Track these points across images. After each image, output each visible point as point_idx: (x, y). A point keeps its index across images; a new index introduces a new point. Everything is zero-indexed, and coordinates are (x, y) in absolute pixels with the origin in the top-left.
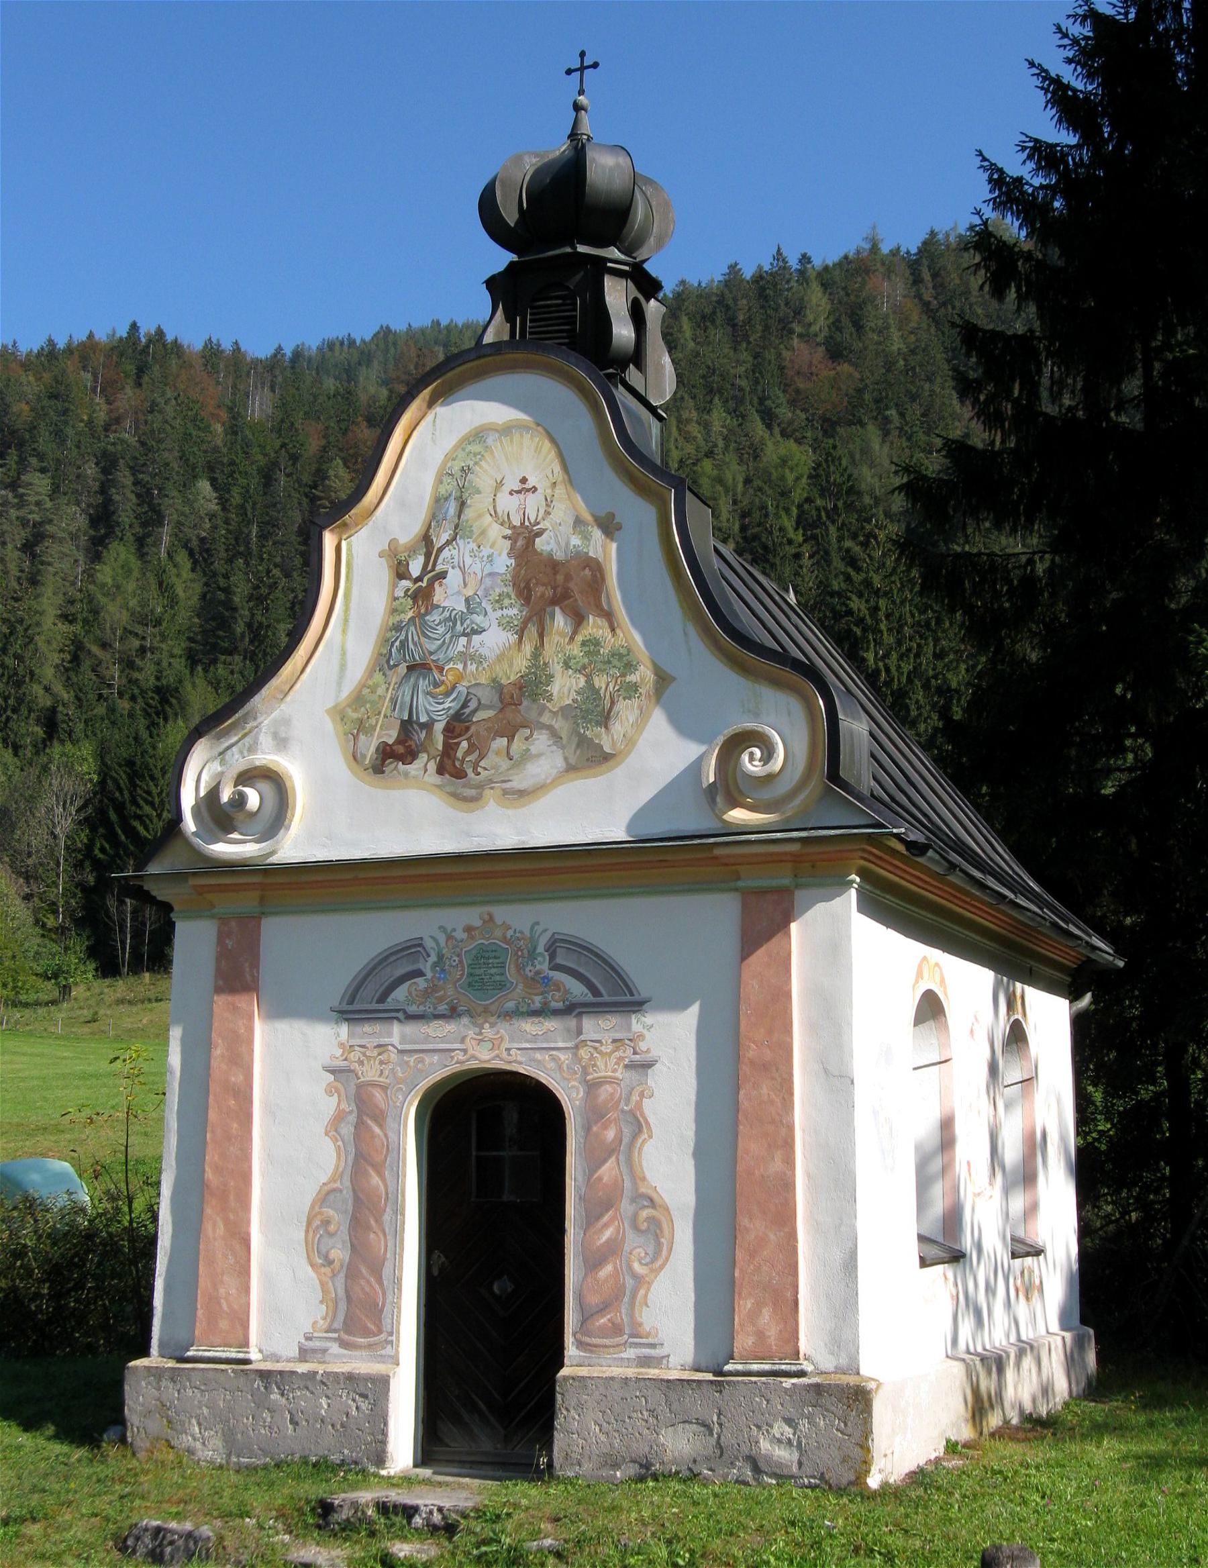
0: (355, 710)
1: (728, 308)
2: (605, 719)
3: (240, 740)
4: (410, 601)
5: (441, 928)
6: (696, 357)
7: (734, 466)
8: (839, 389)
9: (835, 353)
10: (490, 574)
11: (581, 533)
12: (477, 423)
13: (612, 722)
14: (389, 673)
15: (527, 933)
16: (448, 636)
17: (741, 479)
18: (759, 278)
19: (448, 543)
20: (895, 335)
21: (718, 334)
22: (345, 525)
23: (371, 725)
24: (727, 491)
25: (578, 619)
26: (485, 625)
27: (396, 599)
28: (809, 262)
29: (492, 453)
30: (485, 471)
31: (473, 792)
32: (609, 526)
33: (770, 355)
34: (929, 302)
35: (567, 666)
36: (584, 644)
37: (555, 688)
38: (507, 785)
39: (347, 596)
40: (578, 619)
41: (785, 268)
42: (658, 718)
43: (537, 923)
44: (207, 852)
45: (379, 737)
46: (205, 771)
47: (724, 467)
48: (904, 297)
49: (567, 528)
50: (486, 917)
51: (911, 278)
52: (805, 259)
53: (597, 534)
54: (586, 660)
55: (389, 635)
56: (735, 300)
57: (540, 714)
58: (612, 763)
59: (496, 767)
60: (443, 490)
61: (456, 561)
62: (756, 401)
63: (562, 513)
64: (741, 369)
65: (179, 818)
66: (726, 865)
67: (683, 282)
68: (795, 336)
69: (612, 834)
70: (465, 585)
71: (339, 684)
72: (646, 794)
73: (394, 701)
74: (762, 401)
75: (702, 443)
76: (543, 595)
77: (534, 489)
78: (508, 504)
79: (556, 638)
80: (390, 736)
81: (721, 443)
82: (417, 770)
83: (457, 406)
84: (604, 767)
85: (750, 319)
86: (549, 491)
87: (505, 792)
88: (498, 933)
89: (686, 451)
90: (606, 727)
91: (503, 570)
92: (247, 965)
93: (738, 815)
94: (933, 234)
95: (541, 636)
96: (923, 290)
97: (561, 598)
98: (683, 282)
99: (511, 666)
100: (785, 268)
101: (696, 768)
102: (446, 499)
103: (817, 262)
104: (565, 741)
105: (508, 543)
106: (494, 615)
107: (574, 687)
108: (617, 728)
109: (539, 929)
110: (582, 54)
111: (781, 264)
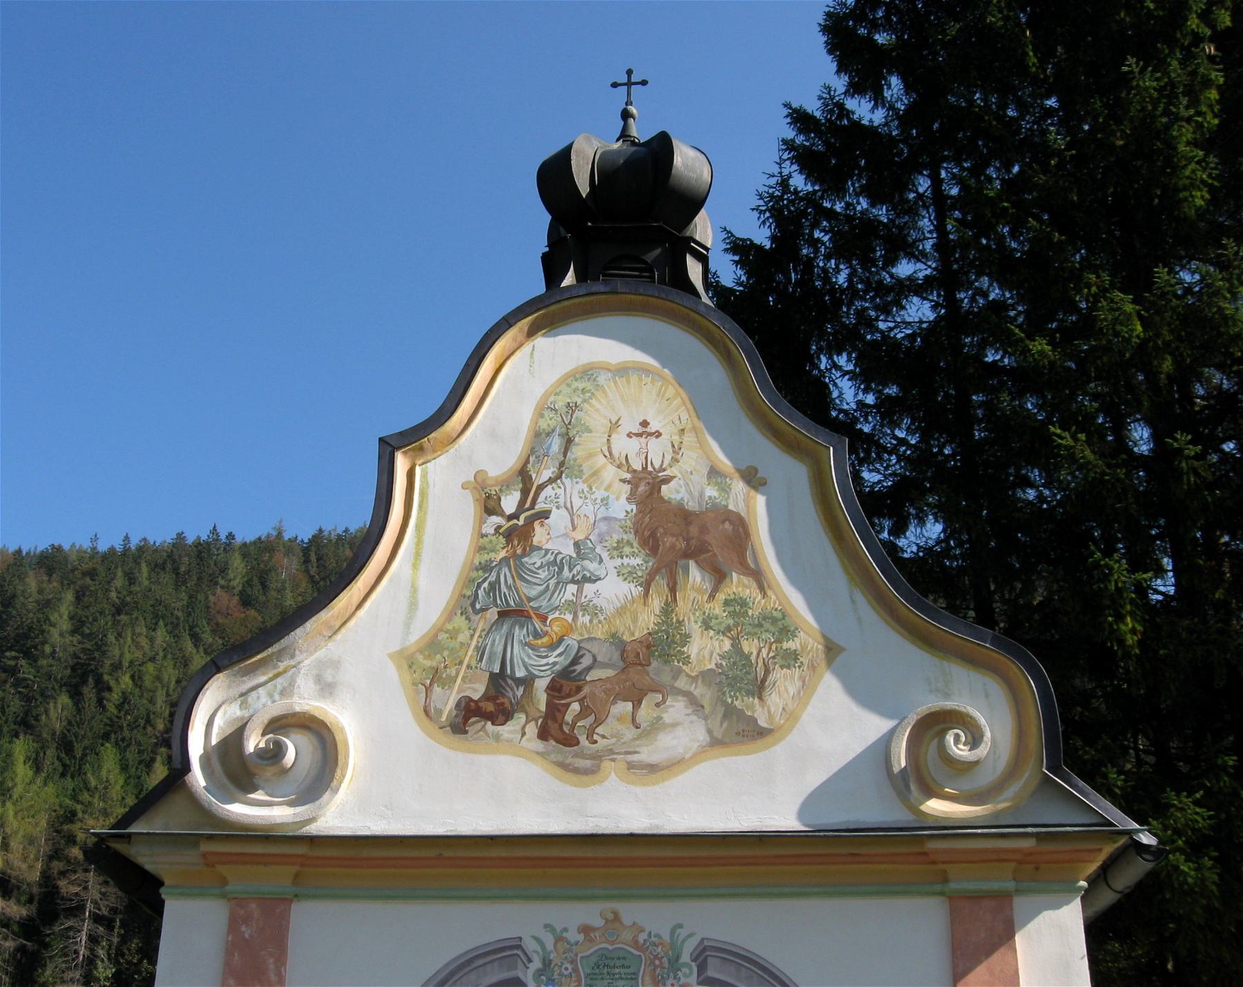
0: (429, 657)
1: (174, 561)
2: (759, 689)
3: (271, 680)
4: (502, 540)
5: (547, 926)
6: (149, 591)
7: (170, 670)
8: (246, 627)
9: (246, 601)
10: (605, 519)
11: (717, 484)
12: (585, 359)
13: (766, 693)
14: (475, 618)
15: (666, 937)
16: (552, 582)
17: (174, 680)
18: (198, 544)
19: (551, 481)
20: (288, 594)
21: (167, 578)
22: (421, 449)
23: (449, 676)
24: (163, 687)
25: (719, 576)
26: (601, 573)
27: (483, 536)
28: (233, 539)
29: (604, 392)
30: (597, 410)
31: (587, 763)
32: (753, 478)
33: (201, 597)
34: (314, 576)
35: (706, 625)
36: (727, 603)
37: (693, 649)
38: (635, 758)
39: (420, 528)
40: (719, 576)
41: (217, 540)
42: (830, 687)
43: (680, 926)
44: (220, 813)
45: (458, 693)
46: (220, 714)
47: (163, 669)
48: (297, 570)
49: (700, 478)
50: (610, 916)
51: (303, 558)
52: (231, 536)
53: (739, 486)
54: (731, 622)
55: (474, 574)
56: (180, 556)
57: (675, 678)
58: (769, 739)
59: (617, 735)
60: (544, 424)
61: (561, 500)
62: (187, 628)
63: (691, 461)
64: (179, 604)
65: (186, 767)
66: (934, 863)
67: (145, 539)
68: (218, 587)
69: (773, 823)
70: (574, 528)
71: (408, 625)
72: (816, 777)
73: (481, 651)
74: (191, 628)
75: (148, 652)
76: (673, 547)
77: (658, 434)
78: (624, 445)
79: (692, 595)
80: (475, 690)
81: (161, 654)
82: (510, 732)
83: (562, 339)
84: (760, 743)
85: (189, 571)
86: (676, 438)
87: (631, 766)
88: (627, 936)
89: (136, 655)
90: (760, 698)
91: (622, 515)
92: (272, 960)
93: (936, 807)
94: (321, 531)
95: (673, 590)
96: (310, 568)
97: (696, 551)
98: (145, 539)
99: (635, 621)
100: (217, 540)
101: (885, 745)
102: (548, 434)
103: (239, 540)
104: (707, 710)
105: (627, 487)
106: (611, 564)
107: (718, 650)
108: (775, 700)
109: (683, 933)
110: (629, 72)
111: (215, 537)
